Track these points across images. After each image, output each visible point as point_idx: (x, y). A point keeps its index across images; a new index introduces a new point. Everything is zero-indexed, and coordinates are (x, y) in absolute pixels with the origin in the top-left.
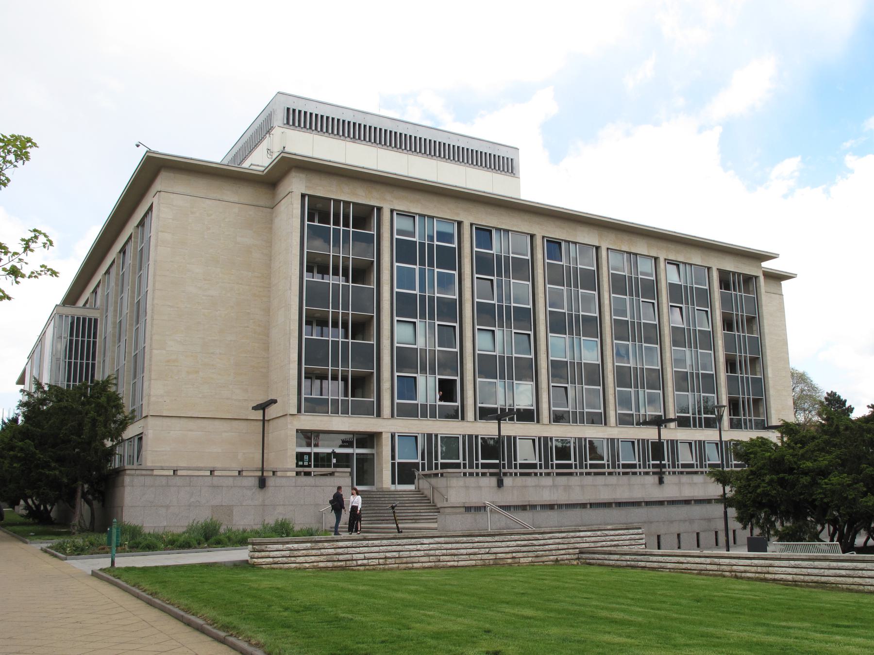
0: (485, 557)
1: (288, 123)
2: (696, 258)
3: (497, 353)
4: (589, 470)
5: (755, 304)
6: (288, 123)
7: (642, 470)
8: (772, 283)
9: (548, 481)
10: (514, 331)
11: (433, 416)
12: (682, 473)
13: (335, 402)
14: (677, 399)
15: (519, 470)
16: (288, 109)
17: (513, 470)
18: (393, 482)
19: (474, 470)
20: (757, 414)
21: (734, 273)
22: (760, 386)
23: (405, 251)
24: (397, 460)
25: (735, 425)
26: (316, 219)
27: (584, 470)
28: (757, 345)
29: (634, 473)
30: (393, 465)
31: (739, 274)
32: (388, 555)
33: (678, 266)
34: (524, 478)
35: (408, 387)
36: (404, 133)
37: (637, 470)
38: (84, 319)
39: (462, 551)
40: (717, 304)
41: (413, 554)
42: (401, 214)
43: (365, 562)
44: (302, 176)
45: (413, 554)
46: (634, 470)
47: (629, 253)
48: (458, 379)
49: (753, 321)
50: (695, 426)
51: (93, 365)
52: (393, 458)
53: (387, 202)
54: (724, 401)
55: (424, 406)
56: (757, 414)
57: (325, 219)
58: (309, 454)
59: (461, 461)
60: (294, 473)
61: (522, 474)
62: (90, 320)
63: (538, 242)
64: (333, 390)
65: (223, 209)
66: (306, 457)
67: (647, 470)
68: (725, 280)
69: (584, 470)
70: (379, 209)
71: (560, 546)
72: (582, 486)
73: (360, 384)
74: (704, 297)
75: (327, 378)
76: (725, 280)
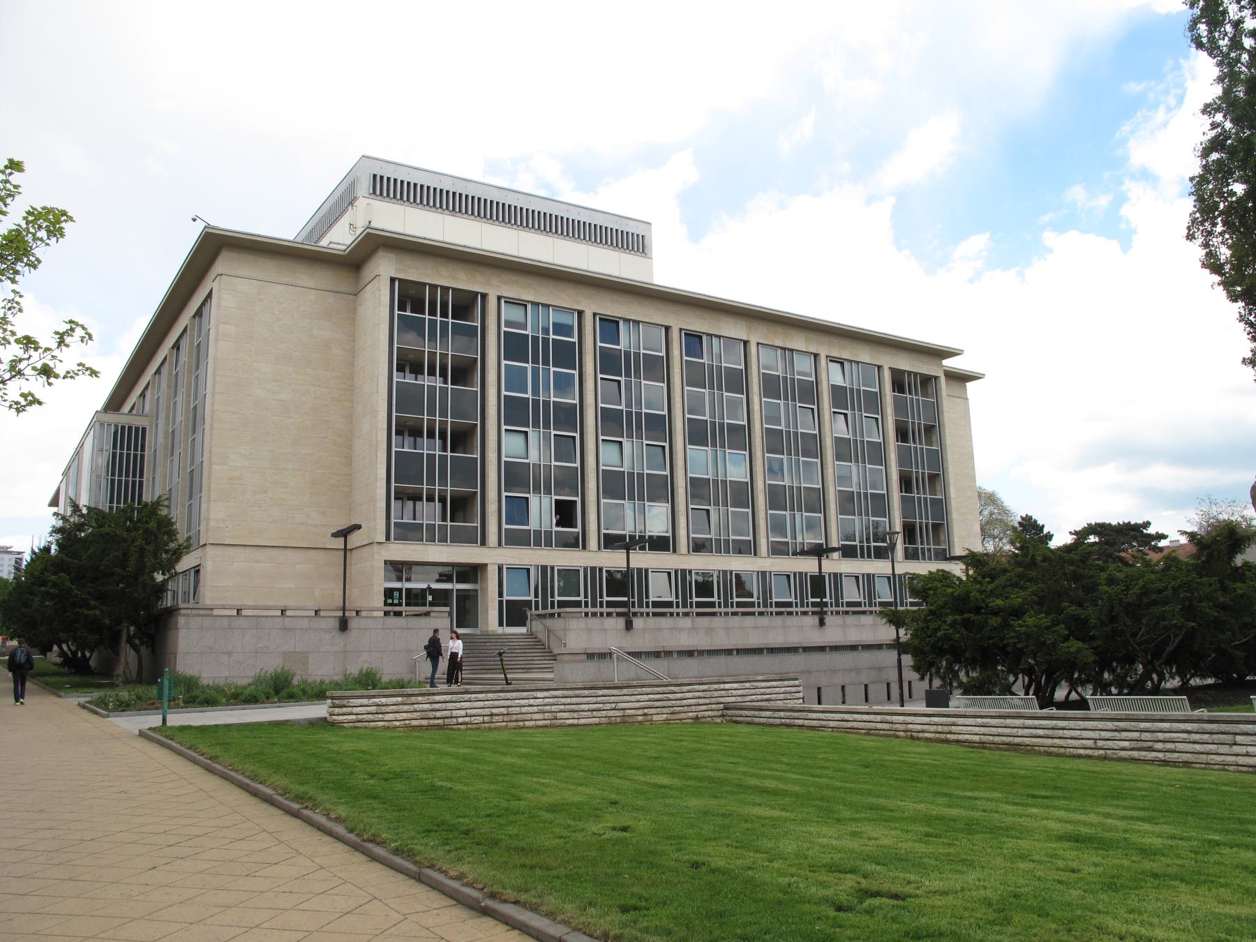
0: (611, 713)
1: (374, 192)
2: (865, 355)
3: (626, 469)
4: (735, 609)
5: (935, 409)
6: (374, 192)
7: (799, 609)
8: (956, 386)
9: (686, 623)
10: (645, 442)
11: (549, 544)
12: (847, 613)
13: (431, 528)
15: (651, 610)
16: (375, 176)
17: (644, 610)
18: (501, 624)
19: (598, 610)
20: (937, 542)
21: (909, 373)
22: (940, 508)
23: (515, 346)
24: (506, 598)
26: (409, 308)
27: (730, 610)
28: (937, 459)
29: (790, 613)
30: (501, 603)
31: (916, 374)
32: (495, 711)
33: (842, 364)
34: (658, 619)
35: (518, 510)
37: (674, 610)
39: (583, 707)
41: (524, 710)
42: (510, 302)
43: (467, 719)
44: (392, 256)
45: (524, 710)
46: (789, 609)
47: (784, 349)
48: (578, 499)
49: (932, 430)
50: (862, 556)
52: (501, 594)
53: (493, 287)
55: (538, 533)
56: (937, 542)
57: (418, 307)
58: (400, 590)
59: (581, 598)
60: (382, 614)
61: (655, 614)
62: (137, 429)
63: (675, 335)
64: (429, 513)
66: (396, 594)
67: (805, 609)
69: (730, 610)
70: (484, 296)
71: (701, 701)
72: (727, 629)
73: (461, 506)
74: (873, 402)
75: (421, 499)
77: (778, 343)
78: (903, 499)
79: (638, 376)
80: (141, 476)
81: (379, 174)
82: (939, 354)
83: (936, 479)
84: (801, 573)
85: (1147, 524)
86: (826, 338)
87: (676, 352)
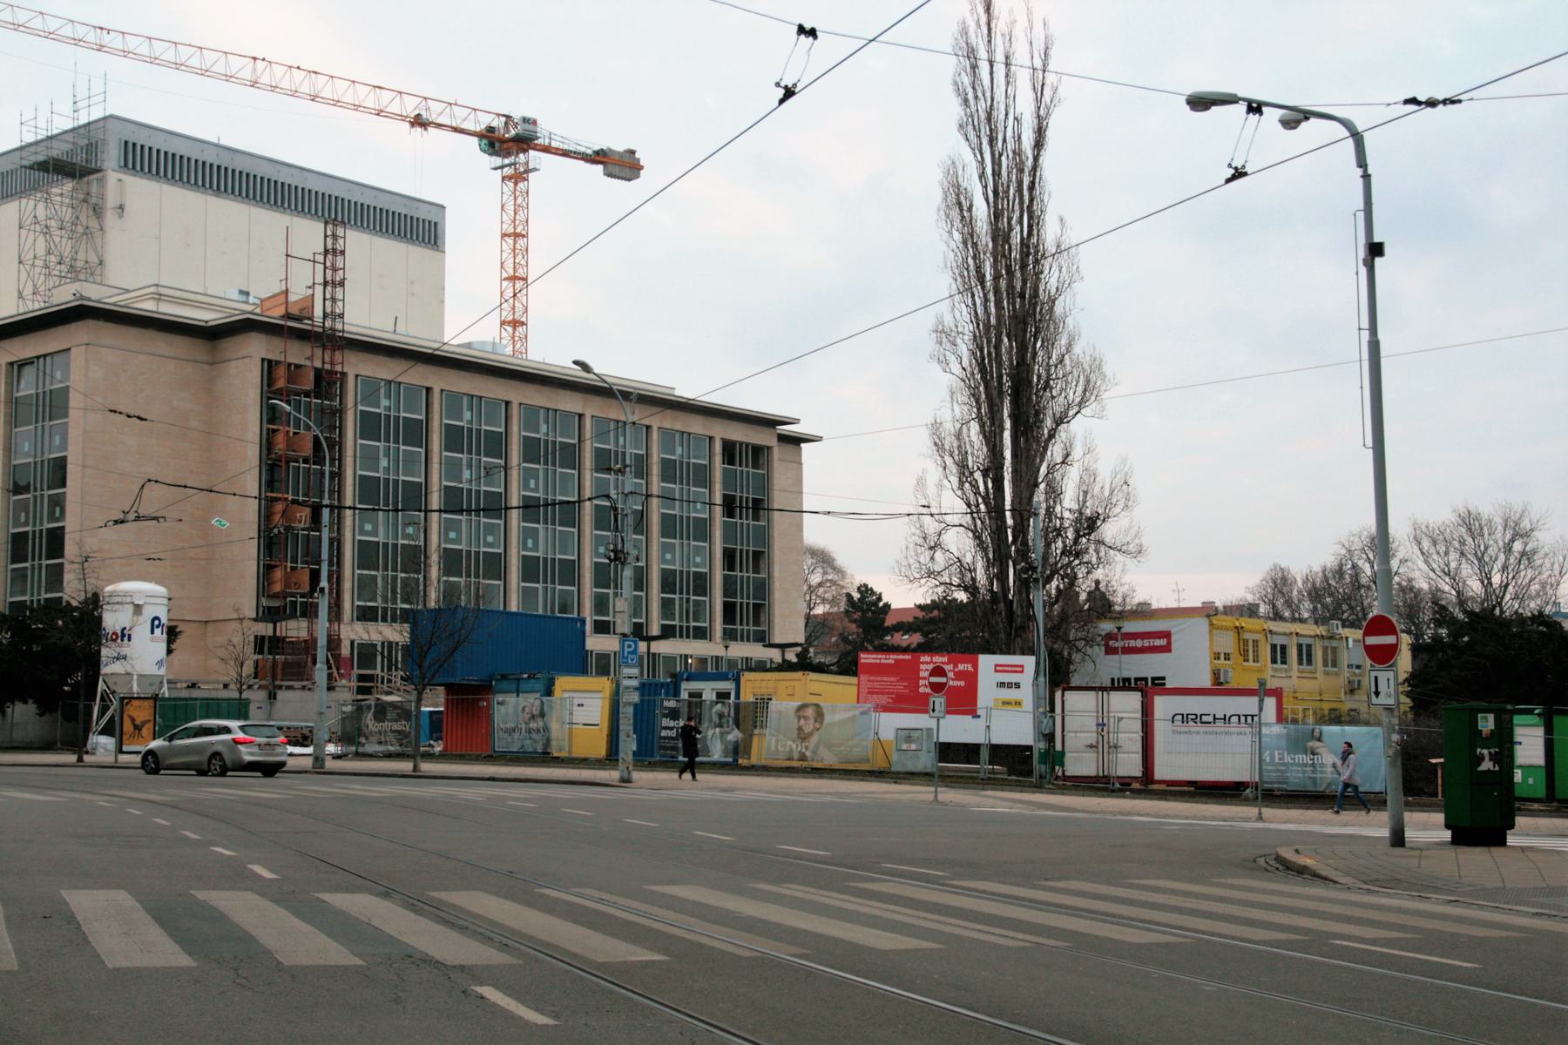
1: (126, 165)
2: (697, 426)
5: (765, 483)
6: (126, 165)
8: (790, 447)
14: (598, 483)
20: (757, 622)
21: (741, 444)
22: (762, 590)
23: (370, 426)
31: (747, 445)
36: (288, 182)
40: (718, 534)
44: (263, 337)
54: (718, 499)
56: (757, 622)
63: (515, 410)
65: (152, 369)
68: (730, 449)
74: (702, 476)
76: (730, 449)
78: (726, 578)
79: (554, 523)
81: (131, 141)
83: (759, 558)
87: (515, 428)
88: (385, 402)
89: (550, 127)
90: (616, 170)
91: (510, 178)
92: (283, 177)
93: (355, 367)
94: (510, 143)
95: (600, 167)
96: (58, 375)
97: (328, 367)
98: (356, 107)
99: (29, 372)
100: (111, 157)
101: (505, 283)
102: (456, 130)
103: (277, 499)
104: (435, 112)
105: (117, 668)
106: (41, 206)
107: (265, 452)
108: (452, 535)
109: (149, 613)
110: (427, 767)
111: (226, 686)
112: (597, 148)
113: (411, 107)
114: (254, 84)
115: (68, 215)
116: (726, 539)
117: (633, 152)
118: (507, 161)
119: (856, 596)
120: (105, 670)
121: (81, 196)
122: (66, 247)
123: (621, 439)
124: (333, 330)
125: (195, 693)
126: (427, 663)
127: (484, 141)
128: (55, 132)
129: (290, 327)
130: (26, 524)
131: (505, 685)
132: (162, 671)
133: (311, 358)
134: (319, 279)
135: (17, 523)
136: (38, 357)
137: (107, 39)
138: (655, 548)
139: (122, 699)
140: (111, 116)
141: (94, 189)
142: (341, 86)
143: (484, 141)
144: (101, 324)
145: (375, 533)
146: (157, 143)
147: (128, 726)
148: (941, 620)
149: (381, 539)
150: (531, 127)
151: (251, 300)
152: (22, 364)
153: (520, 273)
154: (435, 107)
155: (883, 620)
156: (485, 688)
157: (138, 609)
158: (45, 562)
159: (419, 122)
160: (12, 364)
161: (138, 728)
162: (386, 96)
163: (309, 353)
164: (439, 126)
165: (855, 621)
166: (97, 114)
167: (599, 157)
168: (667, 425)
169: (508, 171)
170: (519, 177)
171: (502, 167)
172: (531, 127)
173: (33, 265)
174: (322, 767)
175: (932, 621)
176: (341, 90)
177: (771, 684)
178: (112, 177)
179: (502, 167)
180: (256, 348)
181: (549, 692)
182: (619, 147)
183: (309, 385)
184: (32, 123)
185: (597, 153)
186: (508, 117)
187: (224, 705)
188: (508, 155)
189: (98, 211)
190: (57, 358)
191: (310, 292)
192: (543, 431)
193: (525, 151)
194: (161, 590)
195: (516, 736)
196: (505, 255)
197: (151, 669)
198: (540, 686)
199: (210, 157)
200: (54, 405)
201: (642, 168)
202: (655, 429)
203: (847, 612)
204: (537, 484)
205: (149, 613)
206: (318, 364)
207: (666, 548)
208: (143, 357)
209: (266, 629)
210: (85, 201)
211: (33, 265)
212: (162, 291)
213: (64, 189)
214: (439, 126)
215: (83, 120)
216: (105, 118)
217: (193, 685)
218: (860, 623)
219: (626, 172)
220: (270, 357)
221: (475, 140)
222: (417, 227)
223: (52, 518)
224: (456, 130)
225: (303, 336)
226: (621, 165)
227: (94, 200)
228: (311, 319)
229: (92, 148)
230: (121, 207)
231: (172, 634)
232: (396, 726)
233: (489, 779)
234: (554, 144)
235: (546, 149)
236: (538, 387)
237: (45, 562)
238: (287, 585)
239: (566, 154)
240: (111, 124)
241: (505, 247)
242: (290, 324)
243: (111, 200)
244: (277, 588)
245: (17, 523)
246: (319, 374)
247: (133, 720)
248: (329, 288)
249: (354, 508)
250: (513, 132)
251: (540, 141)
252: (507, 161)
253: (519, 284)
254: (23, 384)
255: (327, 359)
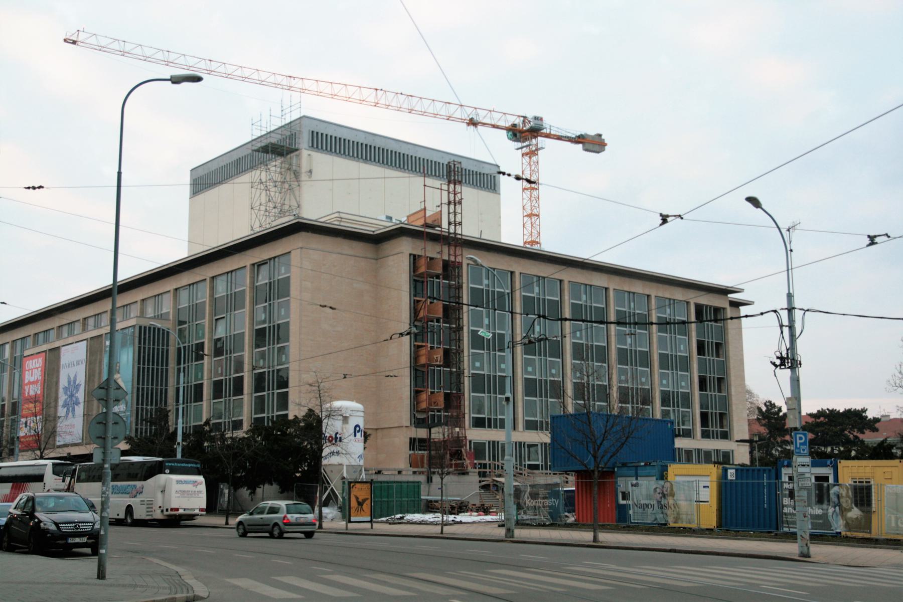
1: (313, 146)
5: (723, 332)
6: (313, 146)
21: (707, 306)
22: (725, 402)
23: (478, 298)
25: (706, 435)
28: (724, 367)
31: (710, 307)
36: (406, 153)
38: (154, 329)
44: (409, 239)
47: (629, 292)
49: (719, 347)
51: (167, 370)
63: (566, 286)
68: (699, 309)
77: (626, 289)
80: (167, 365)
82: (724, 291)
84: (494, 442)
85: (864, 411)
86: (654, 284)
87: (566, 297)
88: (485, 282)
89: (551, 123)
90: (590, 147)
91: (527, 154)
92: (404, 150)
93: (467, 257)
94: (526, 133)
95: (581, 145)
96: (283, 270)
97: (452, 259)
98: (435, 115)
99: (264, 270)
100: (304, 142)
101: (526, 219)
102: (494, 126)
103: (422, 346)
104: (482, 117)
105: (335, 460)
106: (264, 173)
107: (413, 315)
108: (530, 369)
109: (353, 422)
110: (605, 537)
111: (400, 472)
112: (578, 134)
113: (468, 113)
114: (376, 104)
115: (278, 177)
116: (700, 370)
117: (600, 135)
118: (524, 144)
119: (764, 409)
120: (324, 462)
121: (287, 166)
122: (277, 198)
123: (632, 304)
124: (455, 233)
125: (380, 478)
126: (600, 453)
127: (510, 133)
128: (273, 128)
129: (426, 233)
130: (222, 375)
131: (625, 471)
132: (362, 463)
133: (441, 253)
134: (445, 200)
135: (216, 375)
136: (270, 259)
137: (293, 82)
138: (656, 377)
139: (350, 483)
140: (304, 117)
141: (294, 161)
142: (426, 103)
143: (510, 133)
144: (309, 234)
145: (482, 368)
146: (330, 132)
147: (354, 503)
148: (825, 423)
149: (486, 372)
150: (539, 122)
151: (394, 221)
152: (260, 265)
153: (535, 212)
154: (482, 113)
155: (784, 424)
156: (609, 474)
157: (345, 419)
158: (276, 391)
159: (473, 123)
160: (253, 265)
161: (360, 504)
162: (452, 108)
163: (439, 249)
164: (484, 124)
165: (764, 425)
166: (295, 116)
167: (580, 140)
168: (660, 295)
169: (525, 150)
170: (533, 153)
171: (522, 148)
172: (539, 122)
173: (259, 210)
174: (513, 536)
175: (818, 425)
176: (426, 105)
177: (868, 470)
178: (305, 153)
179: (522, 148)
180: (406, 247)
181: (662, 476)
182: (592, 132)
183: (440, 271)
184: (259, 124)
185: (579, 137)
186: (525, 117)
187: (405, 485)
188: (525, 140)
189: (297, 175)
190: (282, 259)
191: (439, 209)
192: (583, 300)
193: (535, 137)
194: (359, 406)
195: (650, 511)
196: (525, 201)
197: (355, 461)
198: (656, 471)
199: (361, 139)
200: (278, 290)
201: (606, 145)
202: (653, 297)
203: (758, 419)
204: (581, 334)
205: (353, 422)
206: (446, 258)
207: (663, 376)
208: (334, 256)
209: (422, 433)
210: (289, 169)
211: (259, 210)
212: (343, 216)
213: (276, 164)
214: (484, 124)
215: (288, 121)
216: (300, 118)
217: (379, 472)
218: (769, 426)
219: (597, 148)
220: (414, 253)
221: (505, 132)
222: (486, 179)
223: (236, 372)
224: (494, 126)
225: (436, 238)
226: (593, 144)
227: (294, 168)
228: (440, 226)
229: (293, 137)
230: (310, 171)
231: (366, 437)
232: (548, 502)
233: (670, 551)
234: (553, 132)
235: (548, 136)
236: (579, 270)
237: (276, 391)
238: (430, 404)
239: (559, 138)
240: (304, 121)
241: (525, 196)
242: (428, 230)
243: (304, 168)
244: (424, 405)
245: (216, 375)
246: (446, 265)
247: (357, 498)
248: (452, 206)
249: (607, 323)
250: (528, 127)
251: (544, 131)
252: (524, 144)
253: (534, 219)
254: (260, 278)
255: (452, 252)
